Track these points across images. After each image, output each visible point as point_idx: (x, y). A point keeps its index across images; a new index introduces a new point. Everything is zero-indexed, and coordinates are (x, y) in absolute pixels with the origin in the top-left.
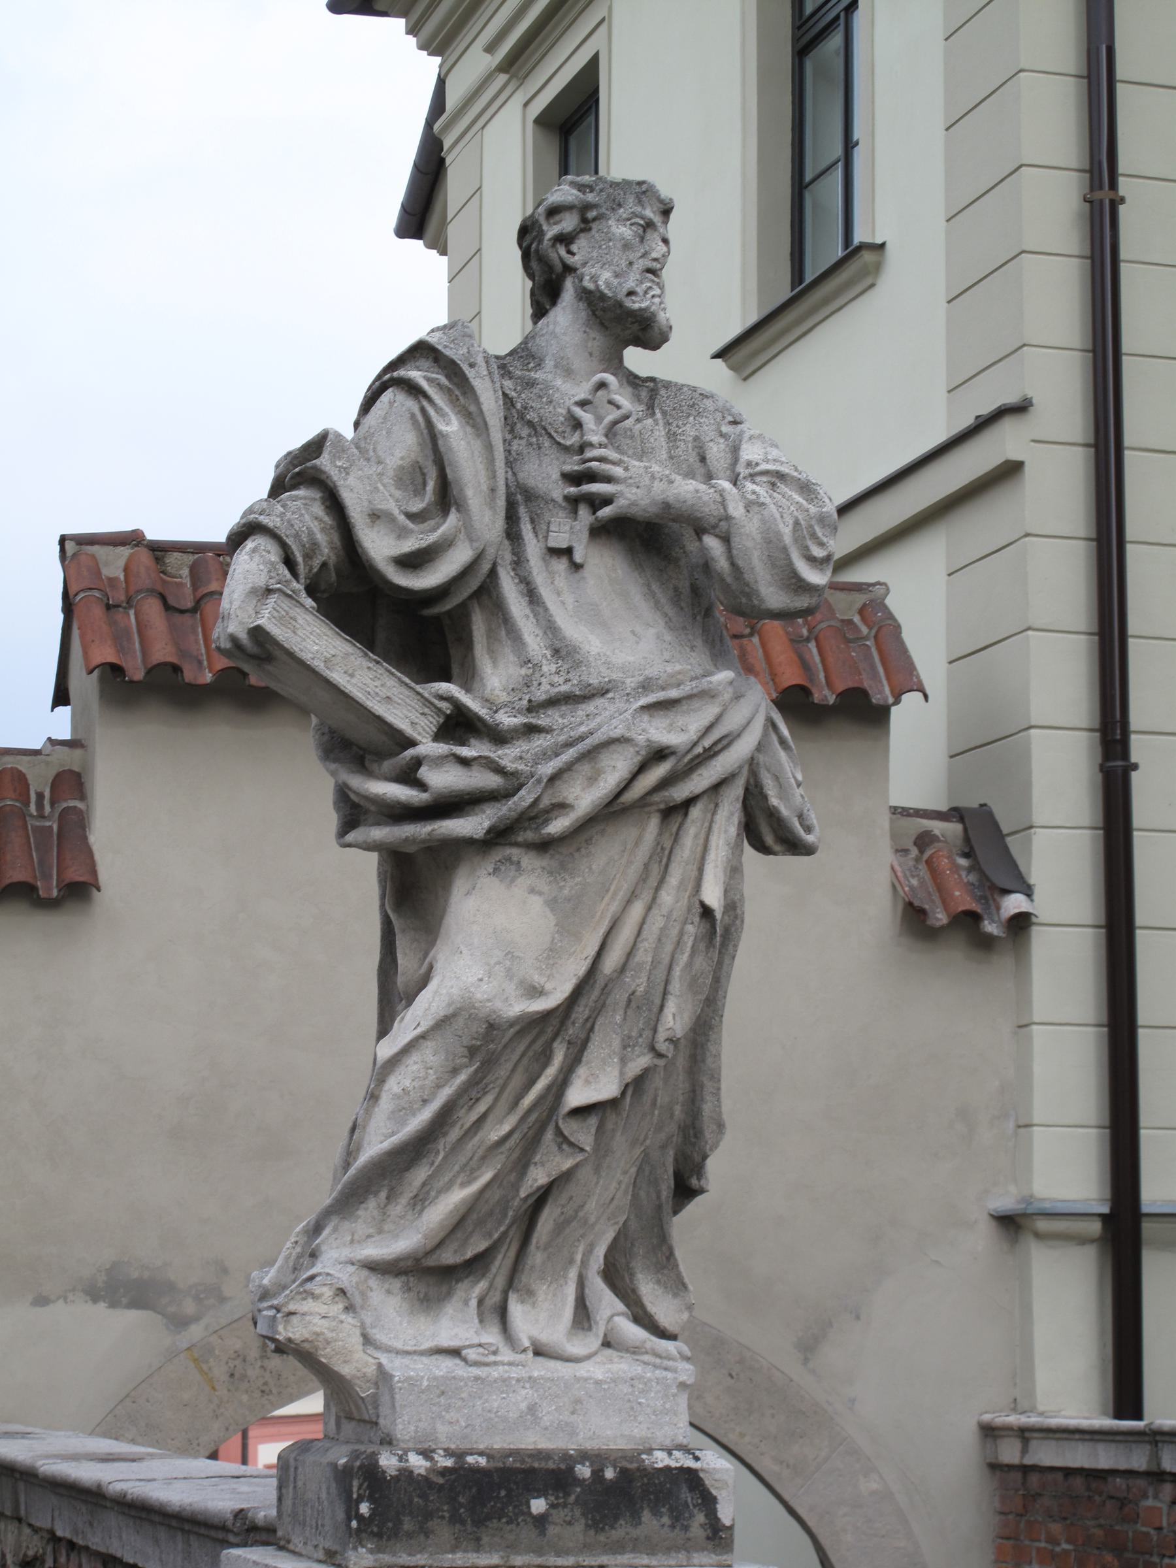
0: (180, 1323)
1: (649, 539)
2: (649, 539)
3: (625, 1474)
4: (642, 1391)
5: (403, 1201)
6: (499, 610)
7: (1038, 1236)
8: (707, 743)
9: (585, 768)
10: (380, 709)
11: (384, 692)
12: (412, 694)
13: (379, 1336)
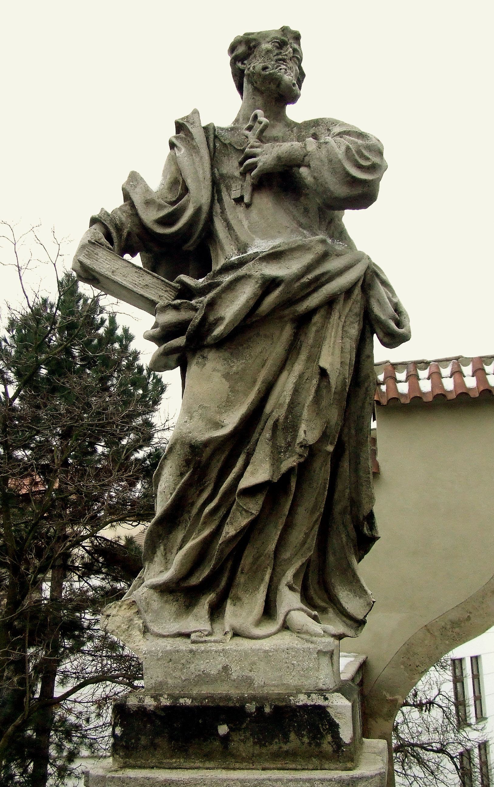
4: (294, 657)
11: (144, 283)
12: (160, 282)
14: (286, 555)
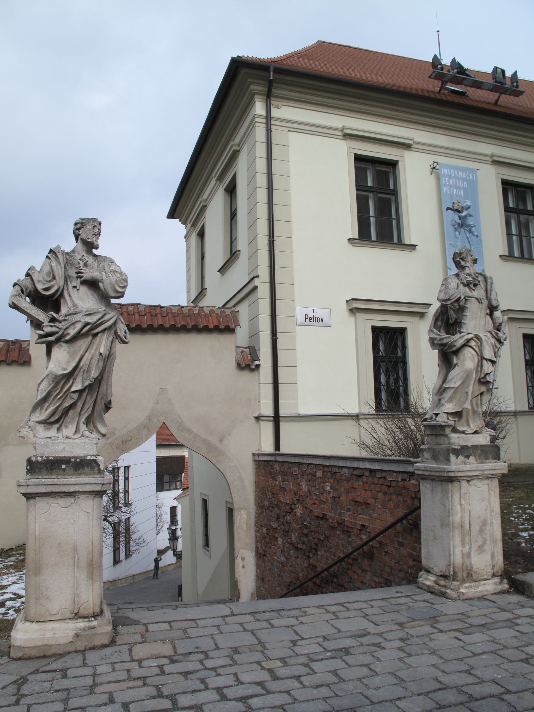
0: (108, 439)
1: (93, 284)
2: (93, 284)
3: (81, 461)
5: (44, 410)
6: (64, 298)
7: (262, 420)
8: (100, 322)
9: (72, 327)
10: (37, 317)
13: (37, 435)
14: (83, 413)
